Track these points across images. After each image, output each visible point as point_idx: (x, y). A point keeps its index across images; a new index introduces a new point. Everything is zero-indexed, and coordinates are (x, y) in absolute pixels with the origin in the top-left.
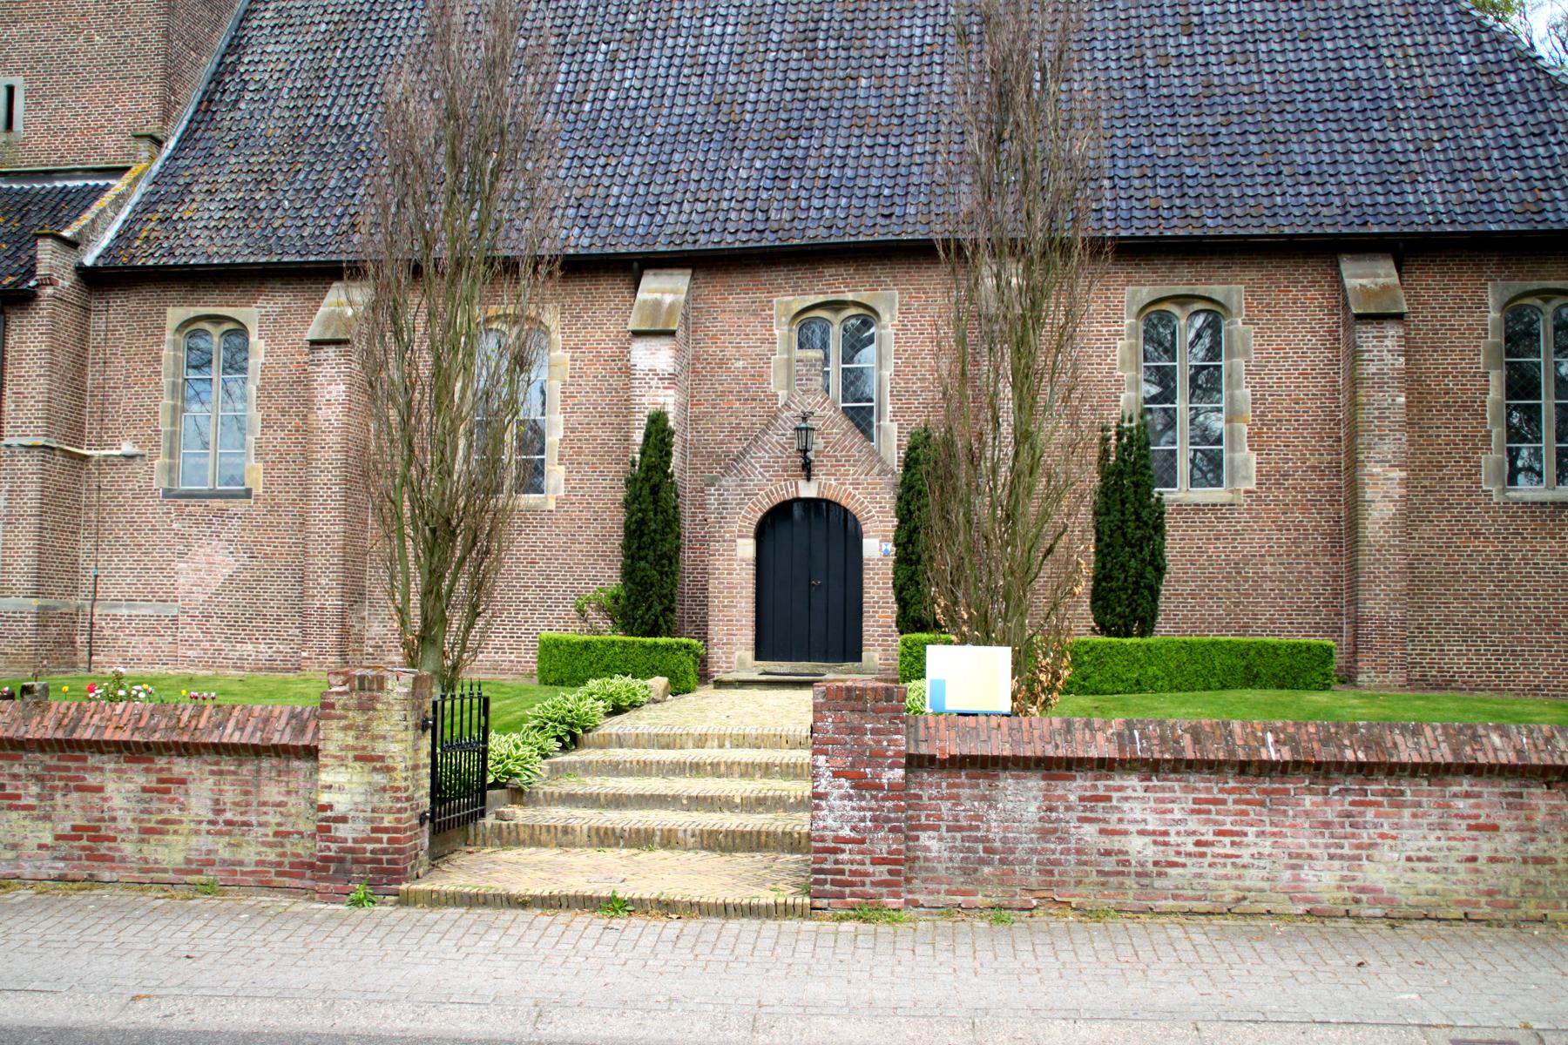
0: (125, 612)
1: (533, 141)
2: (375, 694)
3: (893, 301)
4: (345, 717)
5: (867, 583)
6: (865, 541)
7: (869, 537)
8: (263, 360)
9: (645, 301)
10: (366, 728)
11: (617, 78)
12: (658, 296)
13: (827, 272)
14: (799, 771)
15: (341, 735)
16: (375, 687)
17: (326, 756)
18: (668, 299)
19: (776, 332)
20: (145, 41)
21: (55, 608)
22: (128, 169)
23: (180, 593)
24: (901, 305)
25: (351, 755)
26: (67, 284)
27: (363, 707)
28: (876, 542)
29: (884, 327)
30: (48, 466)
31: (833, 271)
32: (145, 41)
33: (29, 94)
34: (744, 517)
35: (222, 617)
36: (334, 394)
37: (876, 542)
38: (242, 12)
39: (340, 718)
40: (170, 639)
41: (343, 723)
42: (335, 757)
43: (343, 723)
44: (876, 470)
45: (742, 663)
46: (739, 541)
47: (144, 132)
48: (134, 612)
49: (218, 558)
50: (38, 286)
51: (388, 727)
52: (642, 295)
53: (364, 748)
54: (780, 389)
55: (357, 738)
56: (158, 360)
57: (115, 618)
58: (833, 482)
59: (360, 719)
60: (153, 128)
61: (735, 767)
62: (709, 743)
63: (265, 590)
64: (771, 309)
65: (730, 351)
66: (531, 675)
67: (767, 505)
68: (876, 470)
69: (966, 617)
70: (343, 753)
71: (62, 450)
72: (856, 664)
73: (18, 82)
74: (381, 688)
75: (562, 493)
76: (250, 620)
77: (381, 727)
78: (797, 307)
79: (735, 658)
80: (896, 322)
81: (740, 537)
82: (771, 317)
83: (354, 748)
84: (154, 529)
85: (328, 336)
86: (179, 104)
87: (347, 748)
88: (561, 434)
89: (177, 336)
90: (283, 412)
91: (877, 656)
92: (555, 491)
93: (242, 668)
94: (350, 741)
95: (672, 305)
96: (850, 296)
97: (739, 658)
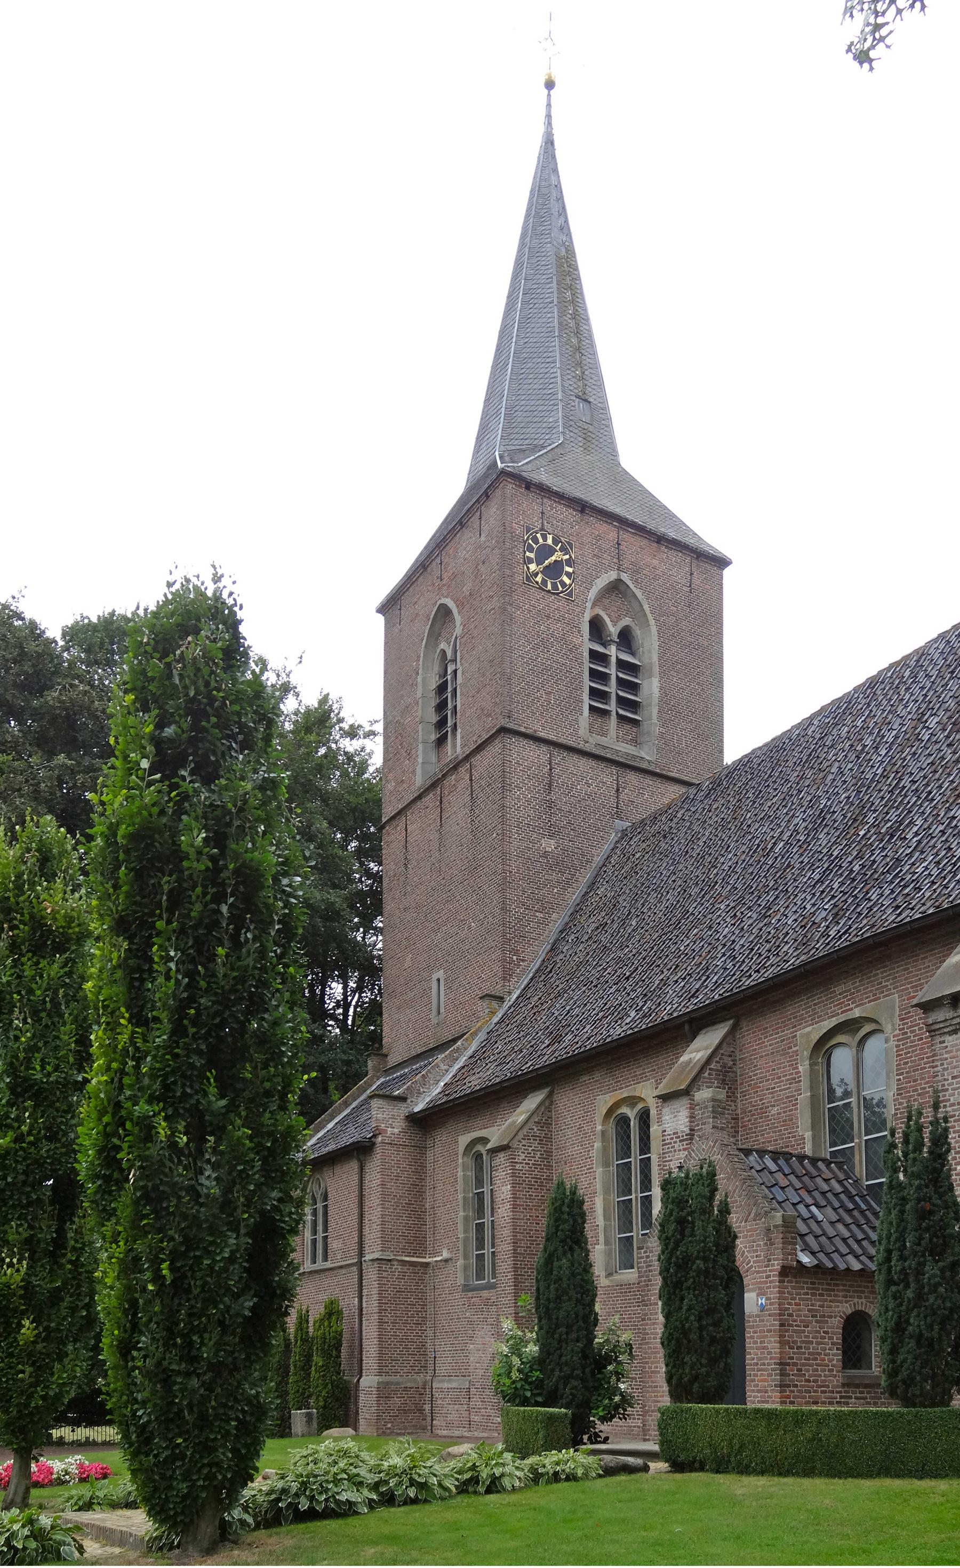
1: (85, 935)
3: (893, 1008)
5: (749, 1344)
6: (747, 1295)
13: (838, 990)
19: (801, 1068)
21: (398, 1384)
24: (901, 1010)
30: (385, 1274)
60: (497, 990)
64: (796, 1045)
71: (397, 1260)
78: (815, 1037)
80: (897, 1032)
89: (466, 1159)
96: (857, 1013)
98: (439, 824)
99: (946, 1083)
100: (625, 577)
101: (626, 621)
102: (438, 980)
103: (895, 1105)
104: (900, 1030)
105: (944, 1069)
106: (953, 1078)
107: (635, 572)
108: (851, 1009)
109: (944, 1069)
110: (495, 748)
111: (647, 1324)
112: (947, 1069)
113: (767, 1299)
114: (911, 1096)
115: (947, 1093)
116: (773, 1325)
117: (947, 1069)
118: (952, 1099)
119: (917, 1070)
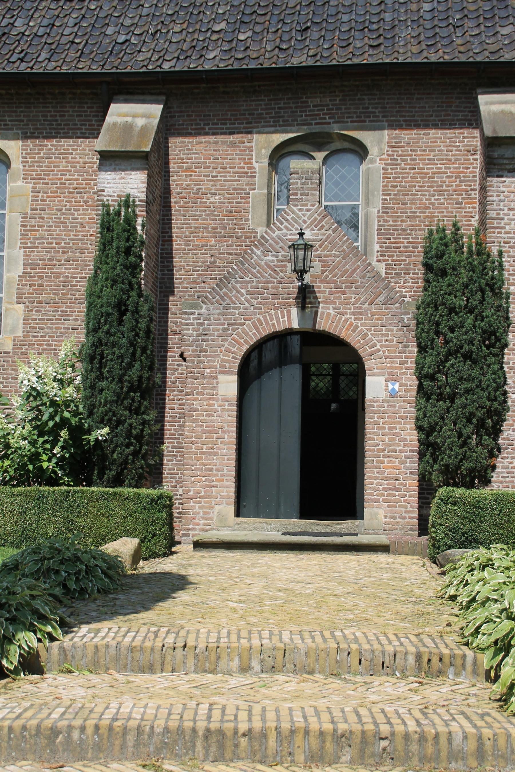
7: (374, 375)
9: (115, 124)
12: (129, 119)
14: (430, 749)
18: (140, 122)
19: (256, 165)
28: (381, 380)
29: (372, 161)
34: (228, 350)
37: (381, 380)
44: (381, 298)
45: (222, 518)
46: (221, 377)
52: (109, 119)
54: (259, 225)
58: (331, 311)
61: (299, 739)
62: (223, 664)
65: (206, 185)
66: (412, 530)
67: (254, 337)
68: (381, 298)
72: (357, 522)
75: (20, 334)
79: (214, 514)
80: (385, 156)
81: (222, 373)
82: (250, 149)
88: (20, 270)
91: (381, 512)
92: (13, 330)
95: (144, 129)
97: (219, 514)
99: (501, 212)
103: (379, 221)
104: (388, 155)
105: (500, 201)
106: (509, 209)
108: (329, 123)
109: (500, 201)
111: (196, 399)
112: (504, 201)
113: (401, 385)
114: (398, 217)
115: (503, 222)
116: (409, 412)
117: (504, 201)
118: (507, 227)
119: (408, 195)
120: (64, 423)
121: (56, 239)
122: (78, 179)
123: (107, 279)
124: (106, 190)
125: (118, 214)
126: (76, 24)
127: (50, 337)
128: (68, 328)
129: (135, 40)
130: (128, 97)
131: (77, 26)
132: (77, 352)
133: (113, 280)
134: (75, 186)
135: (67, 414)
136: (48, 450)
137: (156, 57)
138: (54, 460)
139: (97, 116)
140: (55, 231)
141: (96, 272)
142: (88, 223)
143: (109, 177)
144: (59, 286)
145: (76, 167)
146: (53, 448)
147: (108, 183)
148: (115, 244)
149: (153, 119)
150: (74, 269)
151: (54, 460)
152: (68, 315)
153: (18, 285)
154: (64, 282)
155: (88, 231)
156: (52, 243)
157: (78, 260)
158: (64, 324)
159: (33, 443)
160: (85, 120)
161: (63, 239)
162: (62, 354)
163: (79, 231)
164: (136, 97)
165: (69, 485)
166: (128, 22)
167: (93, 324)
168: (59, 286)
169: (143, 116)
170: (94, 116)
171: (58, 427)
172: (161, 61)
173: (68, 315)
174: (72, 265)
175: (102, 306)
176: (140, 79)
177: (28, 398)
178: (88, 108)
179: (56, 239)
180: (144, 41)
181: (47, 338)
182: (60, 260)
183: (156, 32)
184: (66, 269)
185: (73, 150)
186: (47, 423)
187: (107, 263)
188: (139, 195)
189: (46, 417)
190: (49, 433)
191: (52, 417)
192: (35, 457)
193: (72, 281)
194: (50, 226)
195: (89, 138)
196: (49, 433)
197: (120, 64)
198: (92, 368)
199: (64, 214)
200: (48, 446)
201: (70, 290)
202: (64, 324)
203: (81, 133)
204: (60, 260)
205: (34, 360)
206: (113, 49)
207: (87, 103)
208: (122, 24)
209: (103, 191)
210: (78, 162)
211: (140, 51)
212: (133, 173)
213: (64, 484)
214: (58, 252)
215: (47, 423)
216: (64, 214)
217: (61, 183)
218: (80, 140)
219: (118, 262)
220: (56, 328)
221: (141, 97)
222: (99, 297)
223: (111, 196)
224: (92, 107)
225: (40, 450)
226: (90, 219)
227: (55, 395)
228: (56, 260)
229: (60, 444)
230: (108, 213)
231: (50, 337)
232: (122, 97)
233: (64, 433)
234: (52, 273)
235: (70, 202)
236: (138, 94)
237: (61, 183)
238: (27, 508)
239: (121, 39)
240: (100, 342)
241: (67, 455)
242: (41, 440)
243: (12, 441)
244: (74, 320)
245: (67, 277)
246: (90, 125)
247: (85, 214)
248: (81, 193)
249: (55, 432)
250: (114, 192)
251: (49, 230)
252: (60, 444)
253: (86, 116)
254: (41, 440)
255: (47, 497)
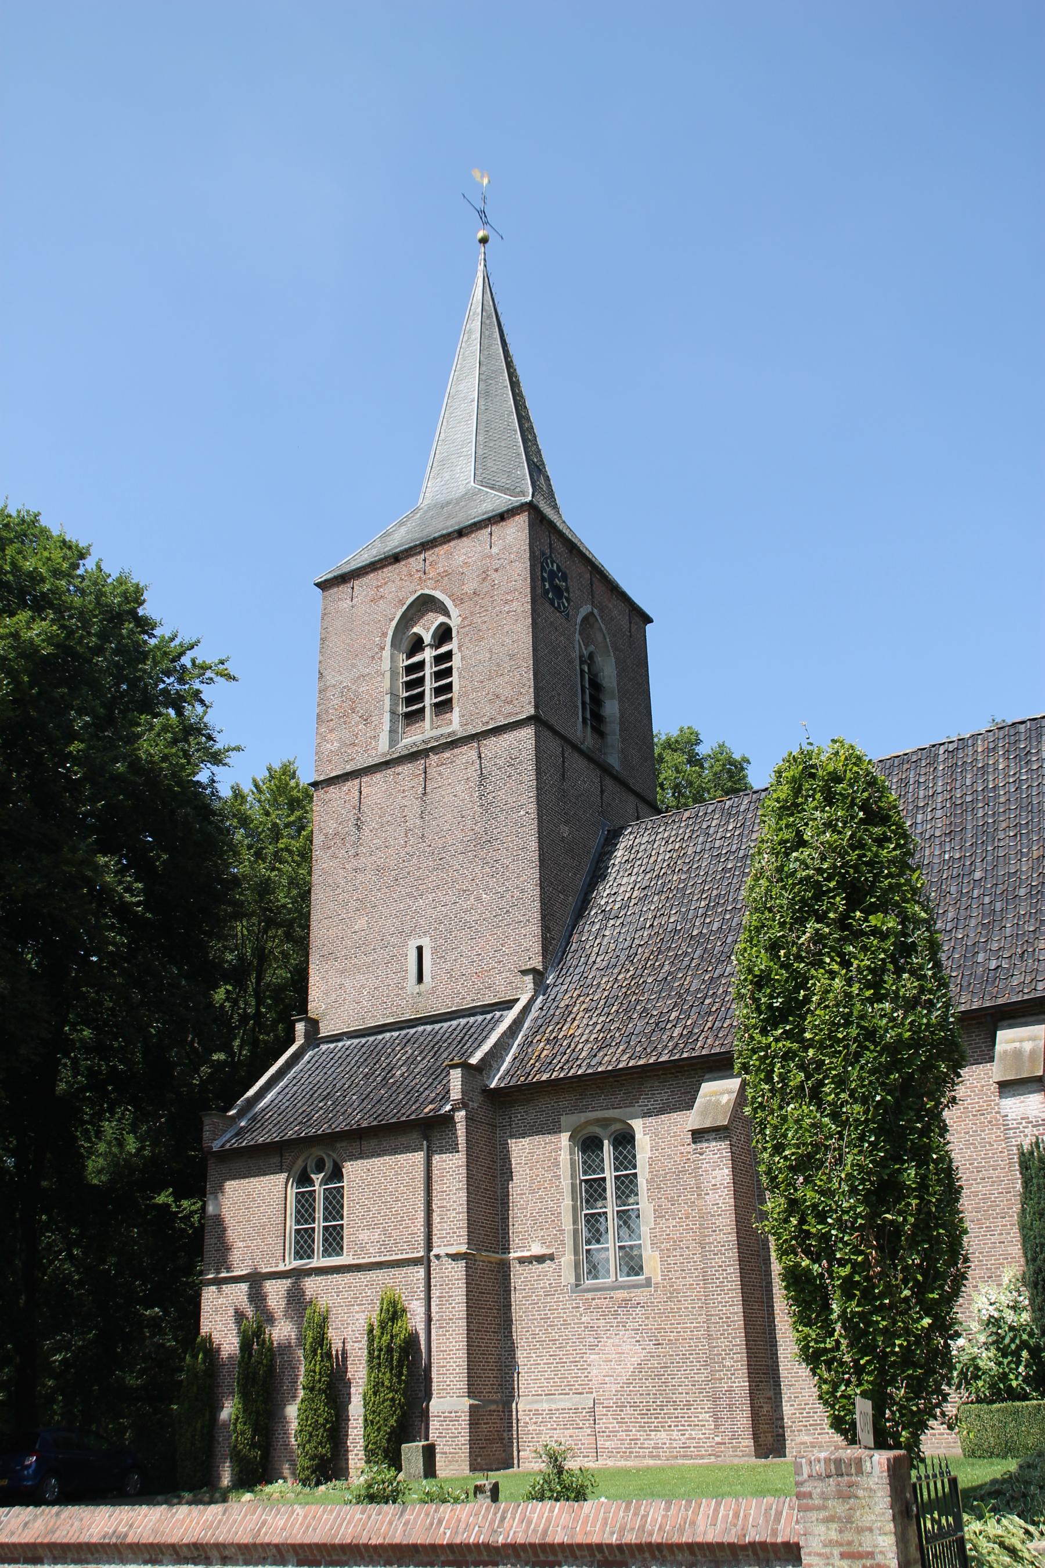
0: (546, 1406)
2: (854, 1478)
4: (824, 1508)
8: (649, 1154)
9: (1005, 1052)
10: (849, 1520)
11: (937, 853)
12: (1017, 1045)
15: (822, 1529)
16: (853, 1471)
17: (809, 1554)
18: (1028, 1046)
20: (522, 891)
22: (518, 999)
23: (594, 1384)
25: (836, 1552)
26: (476, 1105)
27: (844, 1496)
31: (344, 1144)
32: (522, 891)
33: (435, 950)
35: (634, 1406)
36: (719, 1179)
38: (597, 855)
39: (818, 1508)
40: (589, 1431)
41: (823, 1514)
42: (819, 1555)
43: (823, 1514)
47: (528, 967)
48: (554, 1407)
49: (626, 1348)
50: (453, 1110)
51: (874, 1518)
52: (999, 1048)
53: (850, 1543)
55: (841, 1532)
56: (557, 1164)
57: (537, 1413)
59: (839, 1508)
63: (673, 1376)
69: (862, 1362)
70: (827, 1550)
73: (426, 942)
74: (860, 1471)
76: (662, 1407)
77: (867, 1519)
83: (839, 1544)
84: (566, 1324)
85: (707, 1124)
86: (554, 939)
87: (830, 1543)
90: (672, 1201)
93: (658, 1457)
94: (834, 1535)
95: (1033, 1052)
98: (420, 790)
100: (596, 611)
101: (592, 648)
102: (420, 949)
107: (601, 611)
110: (527, 733)
120: (1024, 1345)
121: (968, 1160)
122: (979, 1102)
123: (1034, 1214)
124: (1009, 1115)
125: (1032, 1153)
126: (949, 958)
127: (979, 1253)
128: (995, 1243)
129: (1006, 964)
130: (1011, 1022)
131: (951, 959)
132: (1020, 1277)
133: (1039, 1214)
134: (978, 1108)
135: (1025, 1337)
136: (1014, 1369)
137: (1028, 979)
138: (1020, 1378)
139: (986, 1042)
140: (967, 1153)
141: (1023, 1206)
142: (996, 1141)
143: (1010, 1103)
144: (979, 1203)
145: (974, 1091)
146: (1017, 1368)
147: (1011, 1108)
148: (1035, 1181)
149: (1039, 1042)
150: (990, 1186)
151: (1020, 1378)
152: (993, 1231)
153: (444, 634)
154: (983, 1199)
155: (997, 1149)
156: (966, 1165)
157: (992, 1178)
158: (990, 1239)
159: (999, 1364)
160: (975, 1048)
161: (975, 1160)
162: (1005, 1280)
163: (989, 1150)
164: (1019, 1020)
165: (1037, 1399)
166: (995, 946)
167: (1032, 1255)
168: (979, 1203)
169: (1030, 1039)
170: (983, 1043)
171: (1019, 1348)
172: (1034, 983)
173: (993, 1231)
174: (988, 1182)
175: (1035, 1238)
176: (1018, 1006)
177: (988, 1325)
178: (976, 1036)
179: (968, 1160)
180: (1015, 964)
181: (977, 1255)
182: (976, 1179)
183: (1023, 953)
184: (983, 1187)
185: (969, 1076)
186: (1009, 1345)
187: (1031, 1199)
188: (1040, 1115)
189: (1007, 1341)
190: (1013, 1353)
191: (1013, 1340)
192: (1004, 1377)
193: (991, 1198)
194: (962, 1149)
195: (982, 1063)
196: (1013, 1353)
197: (997, 992)
198: (1037, 1293)
199: (972, 1136)
200: (1013, 1366)
201: (991, 1206)
202: (990, 1239)
203: (974, 1060)
204: (976, 1179)
205: (984, 1288)
206: (987, 977)
207: (974, 1032)
208: (991, 950)
209: (1007, 1116)
210: (976, 1087)
211: (1012, 976)
212: (1031, 1095)
213: (1033, 1398)
214: (973, 1172)
215: (1009, 1345)
216: (972, 1136)
217: (964, 1108)
218: (974, 1066)
219: (1040, 1197)
220: (984, 1244)
221: (1023, 1020)
222: (1031, 1230)
223: (1015, 1120)
224: (980, 1035)
225: (1007, 1370)
226: (996, 1137)
227: (1013, 1321)
228: (973, 1180)
229: (1023, 1363)
230: (1023, 1154)
231: (979, 1253)
232: (1005, 1023)
233: (1025, 1354)
234: (971, 1192)
235: (976, 1124)
236: (1020, 1017)
237: (964, 1108)
238: (1005, 1423)
239: (993, 964)
240: (1040, 1269)
241: (1031, 1373)
242: (1005, 1361)
243: (981, 1364)
244: (999, 1234)
245: (986, 1194)
246: (980, 1051)
247: (991, 1134)
248: (984, 1114)
249: (1017, 1353)
250: (1017, 1116)
251: (961, 1153)
252: (1023, 1363)
253: (975, 1044)
254: (1005, 1361)
255: (1022, 1411)
